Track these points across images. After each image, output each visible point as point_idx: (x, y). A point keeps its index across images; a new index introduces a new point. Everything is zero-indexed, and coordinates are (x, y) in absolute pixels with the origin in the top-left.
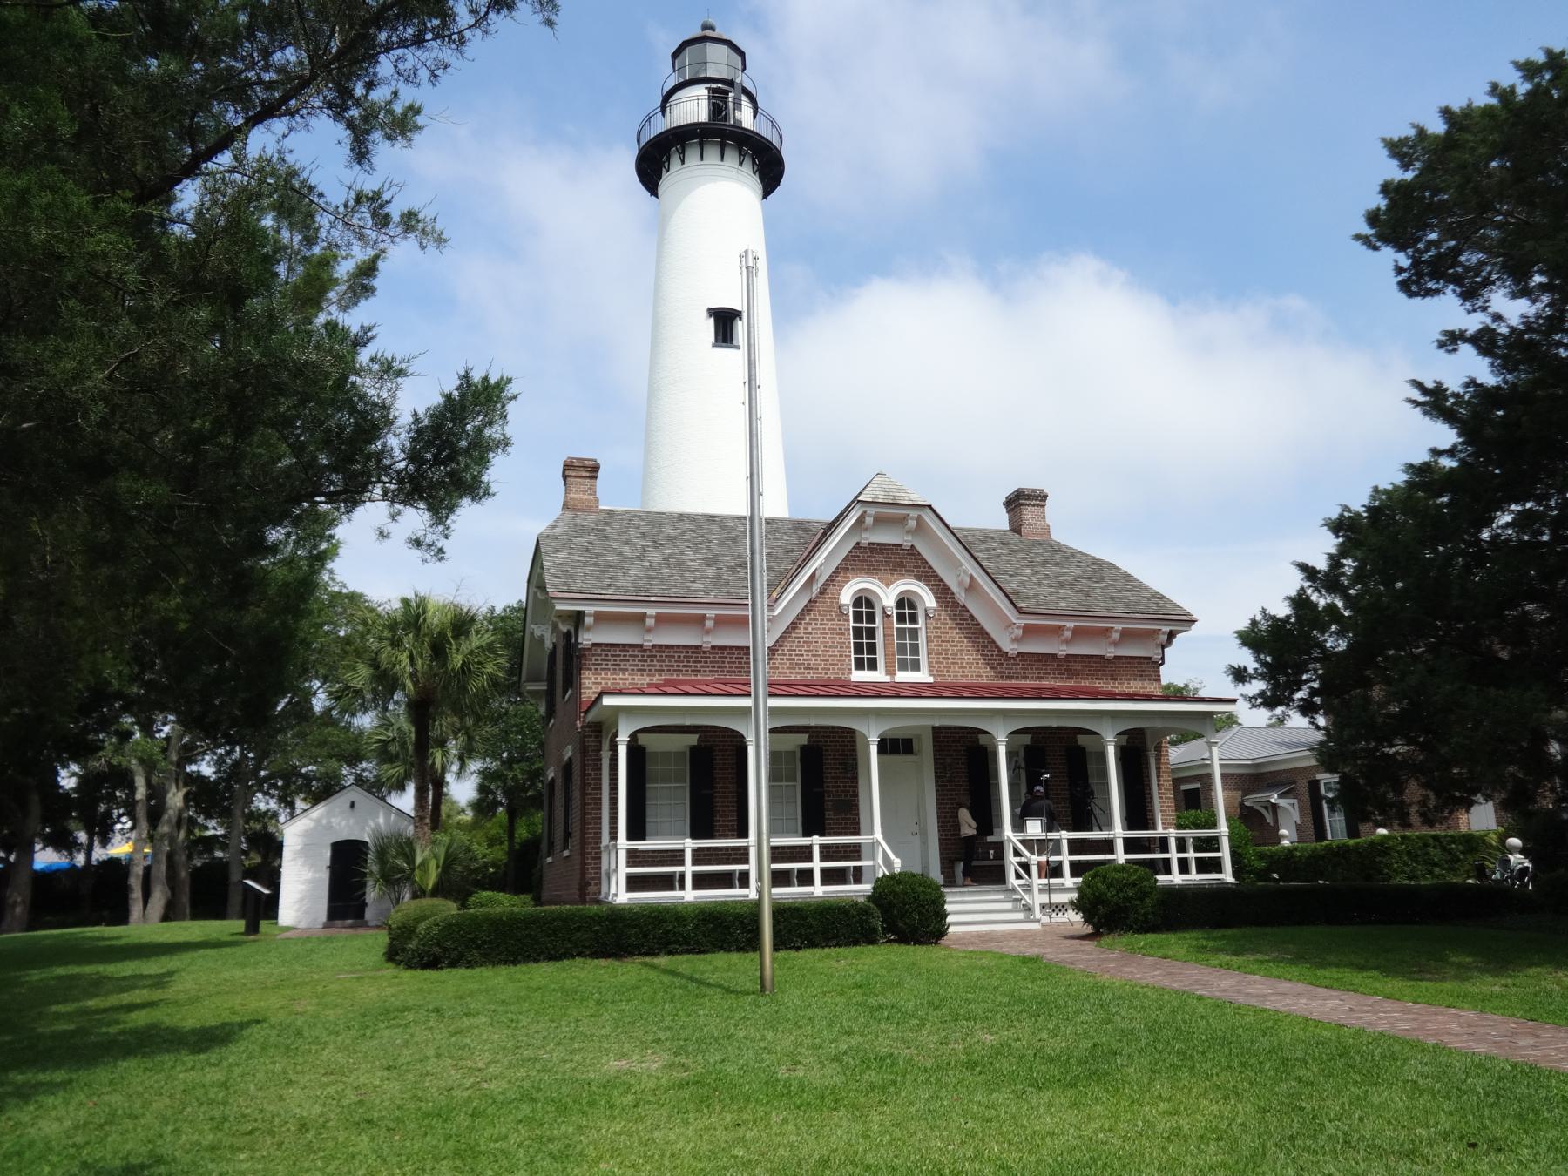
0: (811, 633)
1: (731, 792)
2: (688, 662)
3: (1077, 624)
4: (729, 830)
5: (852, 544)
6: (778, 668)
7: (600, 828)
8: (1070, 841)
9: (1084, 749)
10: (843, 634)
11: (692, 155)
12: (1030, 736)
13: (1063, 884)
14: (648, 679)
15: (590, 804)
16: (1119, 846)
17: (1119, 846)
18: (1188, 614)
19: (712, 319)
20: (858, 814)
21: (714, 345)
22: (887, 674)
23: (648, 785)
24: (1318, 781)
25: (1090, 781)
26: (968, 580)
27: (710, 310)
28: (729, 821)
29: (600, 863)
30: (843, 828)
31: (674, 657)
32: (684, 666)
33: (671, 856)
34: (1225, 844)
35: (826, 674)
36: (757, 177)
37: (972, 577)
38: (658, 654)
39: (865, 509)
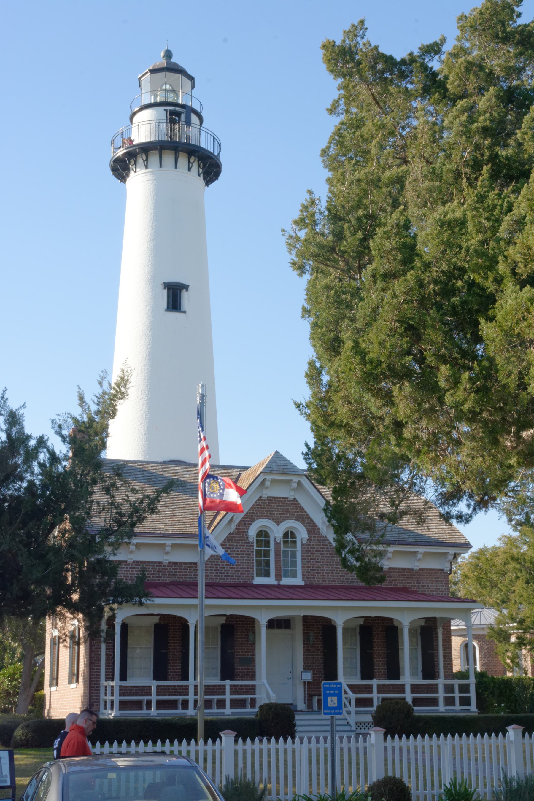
2: (154, 571)
4: (177, 675)
5: (257, 497)
15: (94, 657)
16: (408, 689)
17: (408, 689)
20: (255, 666)
28: (177, 669)
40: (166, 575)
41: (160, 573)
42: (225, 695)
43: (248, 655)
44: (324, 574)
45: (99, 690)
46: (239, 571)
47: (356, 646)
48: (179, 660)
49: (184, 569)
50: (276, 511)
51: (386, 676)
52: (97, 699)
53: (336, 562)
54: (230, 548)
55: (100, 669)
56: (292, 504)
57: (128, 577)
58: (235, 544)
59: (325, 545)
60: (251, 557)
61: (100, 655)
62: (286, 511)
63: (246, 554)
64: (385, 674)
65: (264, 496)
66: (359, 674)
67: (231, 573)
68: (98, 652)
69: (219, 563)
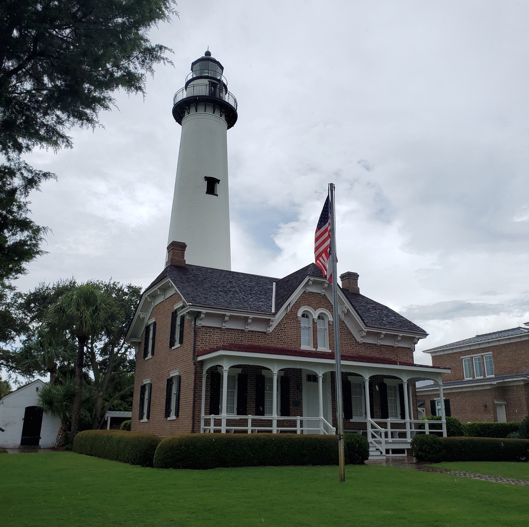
0: (286, 328)
2: (239, 336)
3: (386, 332)
4: (252, 412)
6: (273, 342)
7: (201, 408)
8: (253, 420)
10: (298, 329)
11: (193, 110)
12: (284, 372)
15: (197, 397)
16: (275, 423)
17: (275, 423)
18: (424, 331)
20: (302, 407)
21: (207, 193)
22: (330, 349)
24: (435, 401)
25: (388, 398)
26: (346, 311)
27: (205, 177)
28: (252, 407)
29: (200, 424)
30: (296, 413)
31: (233, 334)
35: (291, 345)
36: (223, 118)
37: (348, 310)
38: (220, 332)
41: (243, 338)
44: (343, 346)
45: (200, 422)
46: (292, 340)
50: (313, 302)
51: (381, 417)
53: (349, 339)
56: (322, 298)
57: (222, 339)
60: (299, 331)
62: (319, 302)
63: (296, 329)
64: (380, 416)
66: (235, 411)
68: (200, 393)
69: (279, 333)
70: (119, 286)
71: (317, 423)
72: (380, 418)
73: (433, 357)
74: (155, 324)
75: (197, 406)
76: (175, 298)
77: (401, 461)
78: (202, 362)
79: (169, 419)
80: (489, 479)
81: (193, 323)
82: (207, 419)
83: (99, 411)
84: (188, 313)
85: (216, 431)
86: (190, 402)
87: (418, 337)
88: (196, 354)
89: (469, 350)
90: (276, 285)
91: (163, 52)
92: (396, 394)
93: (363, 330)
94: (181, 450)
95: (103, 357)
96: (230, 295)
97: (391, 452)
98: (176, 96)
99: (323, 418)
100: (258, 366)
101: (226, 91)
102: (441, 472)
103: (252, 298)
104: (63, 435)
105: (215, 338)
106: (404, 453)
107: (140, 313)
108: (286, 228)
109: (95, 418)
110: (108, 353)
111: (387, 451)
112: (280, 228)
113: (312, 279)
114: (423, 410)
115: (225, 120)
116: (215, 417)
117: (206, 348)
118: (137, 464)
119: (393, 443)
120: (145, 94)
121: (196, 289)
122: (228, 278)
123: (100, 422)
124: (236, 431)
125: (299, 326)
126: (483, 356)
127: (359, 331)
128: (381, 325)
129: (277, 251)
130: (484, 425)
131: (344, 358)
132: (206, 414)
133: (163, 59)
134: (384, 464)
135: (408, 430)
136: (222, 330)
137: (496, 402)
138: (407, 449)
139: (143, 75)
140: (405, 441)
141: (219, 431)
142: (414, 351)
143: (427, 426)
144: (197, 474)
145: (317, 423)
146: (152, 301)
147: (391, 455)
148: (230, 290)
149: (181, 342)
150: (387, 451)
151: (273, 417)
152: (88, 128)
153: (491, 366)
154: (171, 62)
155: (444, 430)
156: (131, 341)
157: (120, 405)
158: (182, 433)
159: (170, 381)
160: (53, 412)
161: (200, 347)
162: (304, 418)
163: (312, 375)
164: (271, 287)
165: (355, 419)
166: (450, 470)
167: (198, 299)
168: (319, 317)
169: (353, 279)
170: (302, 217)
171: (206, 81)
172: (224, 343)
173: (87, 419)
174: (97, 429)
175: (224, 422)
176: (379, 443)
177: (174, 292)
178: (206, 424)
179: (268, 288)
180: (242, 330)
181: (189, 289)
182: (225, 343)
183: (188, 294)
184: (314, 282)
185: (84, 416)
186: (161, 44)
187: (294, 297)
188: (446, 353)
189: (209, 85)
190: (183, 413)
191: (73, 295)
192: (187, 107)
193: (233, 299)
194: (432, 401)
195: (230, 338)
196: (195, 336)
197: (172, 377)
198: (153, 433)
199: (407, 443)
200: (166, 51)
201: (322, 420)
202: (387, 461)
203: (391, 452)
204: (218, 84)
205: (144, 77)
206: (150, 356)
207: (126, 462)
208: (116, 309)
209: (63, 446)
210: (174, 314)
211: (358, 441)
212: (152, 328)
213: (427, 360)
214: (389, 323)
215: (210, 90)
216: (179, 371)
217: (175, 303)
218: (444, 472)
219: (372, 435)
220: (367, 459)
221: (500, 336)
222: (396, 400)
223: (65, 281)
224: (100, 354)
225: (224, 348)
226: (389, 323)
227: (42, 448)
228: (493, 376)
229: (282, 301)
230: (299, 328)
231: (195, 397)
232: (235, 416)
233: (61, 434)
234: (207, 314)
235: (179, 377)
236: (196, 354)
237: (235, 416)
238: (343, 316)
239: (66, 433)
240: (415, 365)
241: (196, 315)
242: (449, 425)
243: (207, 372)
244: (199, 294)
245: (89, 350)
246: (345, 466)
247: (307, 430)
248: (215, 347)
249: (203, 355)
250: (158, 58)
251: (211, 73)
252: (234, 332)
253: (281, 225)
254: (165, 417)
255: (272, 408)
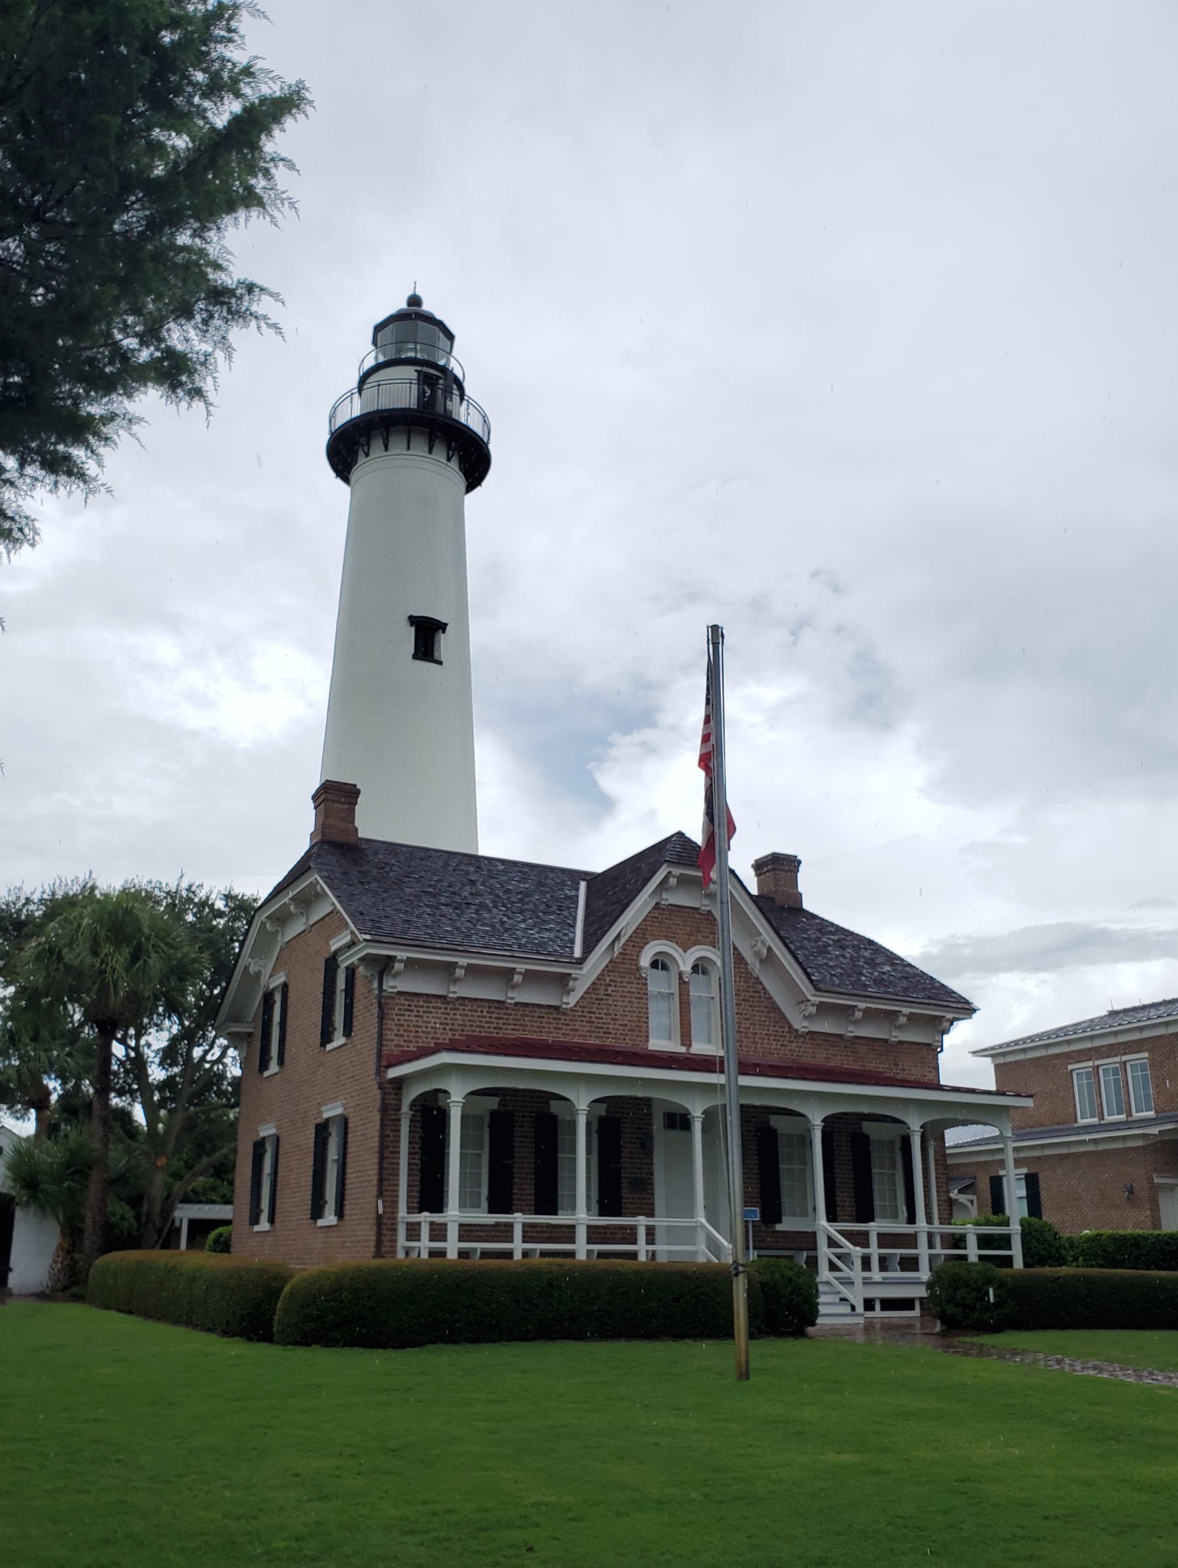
1: (529, 1163)
4: (527, 1205)
5: (653, 904)
9: (556, 1117)
10: (641, 998)
12: (497, 1099)
13: (920, 1278)
14: (450, 1033)
15: (388, 1169)
16: (581, 1234)
17: (581, 1234)
18: (967, 1002)
19: (413, 630)
20: (653, 1194)
21: (416, 656)
22: (682, 1044)
23: (559, 1155)
25: (781, 1166)
26: (765, 951)
28: (528, 1195)
29: (396, 1235)
31: (476, 1011)
32: (486, 1022)
33: (468, 1231)
34: (1017, 1242)
36: (454, 464)
37: (769, 949)
39: (671, 869)
40: (509, 1024)
41: (501, 1021)
42: (635, 1242)
43: (641, 1173)
45: (395, 1230)
47: (482, 1149)
48: (531, 1179)
49: (539, 1017)
51: (532, 1208)
52: (391, 1247)
54: (611, 986)
55: (398, 1191)
57: (448, 1024)
58: (619, 980)
59: (757, 992)
61: (398, 1164)
65: (663, 902)
66: (484, 1204)
67: (613, 1029)
68: (395, 1158)
70: (202, 894)
71: (689, 1234)
72: (851, 1221)
73: (997, 1067)
74: (285, 987)
75: (387, 1191)
76: (331, 924)
77: (905, 1329)
78: (399, 1083)
79: (320, 1223)
80: (1120, 1373)
81: (376, 985)
82: (412, 1224)
83: (157, 1207)
84: (361, 959)
85: (433, 1253)
86: (371, 1181)
87: (949, 1016)
88: (385, 1061)
89: (1090, 1049)
90: (588, 888)
91: (255, 299)
92: (893, 1160)
93: (808, 1001)
94: (342, 1302)
95: (167, 1070)
96: (470, 913)
97: (878, 1306)
98: (332, 416)
99: (703, 1220)
100: (541, 1092)
101: (462, 395)
102: (1001, 1356)
103: (524, 921)
104: (66, 1263)
105: (430, 1022)
106: (912, 1308)
107: (249, 960)
108: (625, 745)
109: (147, 1222)
110: (180, 1059)
111: (869, 1304)
112: (610, 745)
113: (676, 871)
114: (972, 1202)
115: (461, 470)
116: (432, 1219)
117: (408, 1047)
118: (234, 1335)
119: (884, 1283)
120: (211, 408)
121: (383, 900)
122: (468, 873)
123: (160, 1231)
124: (485, 1254)
125: (644, 991)
126: (1125, 1063)
127: (799, 1003)
128: (853, 988)
129: (604, 804)
130: (1124, 1237)
131: (745, 1068)
132: (410, 1210)
133: (256, 317)
134: (860, 1338)
135: (923, 1251)
136: (448, 1003)
137: (1156, 1180)
138: (921, 1299)
139: (210, 355)
140: (916, 1278)
141: (441, 1253)
142: (942, 1051)
143: (972, 1242)
144: (378, 1361)
145: (689, 1234)
146: (277, 931)
147: (878, 1313)
148: (470, 901)
149: (348, 1032)
150: (869, 1304)
151: (577, 1220)
152: (70, 492)
153: (1146, 1088)
154: (275, 326)
155: (1016, 1252)
156: (228, 1031)
157: (214, 1189)
158: (353, 1258)
159: (322, 1130)
160: (42, 1208)
161: (393, 1043)
162: (658, 1222)
163: (678, 1112)
164: (573, 893)
165: (787, 1225)
166: (1024, 1352)
167: (386, 926)
168: (695, 969)
169: (787, 872)
170: (667, 718)
171: (410, 372)
172: (454, 1035)
173: (126, 1224)
174: (153, 1248)
175: (453, 1232)
176: (848, 1282)
177: (330, 909)
178: (411, 1235)
179: (566, 895)
180: (499, 1002)
181: (365, 899)
182: (457, 1033)
183: (362, 914)
184: (683, 881)
185: (118, 1217)
186: (252, 278)
187: (629, 916)
188: (1030, 1055)
189: (418, 380)
190: (354, 1209)
191: (82, 918)
192: (363, 440)
193: (475, 925)
194: (995, 1177)
195: (469, 1021)
196: (382, 1016)
197: (328, 1120)
198: (283, 1259)
199: (916, 1283)
200: (264, 297)
201: (702, 1226)
202: (869, 1327)
203: (878, 1306)
204: (441, 378)
205: (213, 361)
206: (274, 1067)
207: (209, 1330)
208: (189, 951)
209: (65, 1288)
210: (331, 964)
211: (790, 1280)
212: (278, 998)
213: (984, 1077)
214: (878, 982)
215: (421, 394)
216: (343, 1105)
217: (333, 935)
218: (1008, 1356)
219: (831, 1263)
220: (813, 1324)
221: (1169, 1012)
222: (894, 1174)
223: (70, 883)
224: (161, 1064)
225: (453, 1047)
226: (878, 982)
227: (15, 1292)
228: (1151, 1114)
229: (599, 928)
230: (642, 996)
231: (381, 1169)
232: (482, 1217)
233: (60, 1259)
234: (409, 963)
235: (344, 1121)
236: (385, 1061)
237: (482, 1217)
238: (758, 965)
239: (72, 1259)
240: (941, 1088)
241: (384, 965)
242: (1028, 1237)
243: (413, 1104)
244: (390, 911)
245: (132, 1054)
246: (750, 1342)
247: (665, 1251)
248: (432, 1045)
249: (401, 1063)
250: (237, 315)
251: (422, 351)
252: (478, 1006)
253: (615, 737)
254: (312, 1218)
255: (575, 1196)
